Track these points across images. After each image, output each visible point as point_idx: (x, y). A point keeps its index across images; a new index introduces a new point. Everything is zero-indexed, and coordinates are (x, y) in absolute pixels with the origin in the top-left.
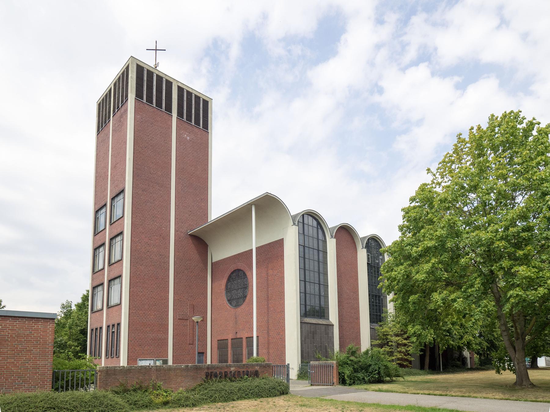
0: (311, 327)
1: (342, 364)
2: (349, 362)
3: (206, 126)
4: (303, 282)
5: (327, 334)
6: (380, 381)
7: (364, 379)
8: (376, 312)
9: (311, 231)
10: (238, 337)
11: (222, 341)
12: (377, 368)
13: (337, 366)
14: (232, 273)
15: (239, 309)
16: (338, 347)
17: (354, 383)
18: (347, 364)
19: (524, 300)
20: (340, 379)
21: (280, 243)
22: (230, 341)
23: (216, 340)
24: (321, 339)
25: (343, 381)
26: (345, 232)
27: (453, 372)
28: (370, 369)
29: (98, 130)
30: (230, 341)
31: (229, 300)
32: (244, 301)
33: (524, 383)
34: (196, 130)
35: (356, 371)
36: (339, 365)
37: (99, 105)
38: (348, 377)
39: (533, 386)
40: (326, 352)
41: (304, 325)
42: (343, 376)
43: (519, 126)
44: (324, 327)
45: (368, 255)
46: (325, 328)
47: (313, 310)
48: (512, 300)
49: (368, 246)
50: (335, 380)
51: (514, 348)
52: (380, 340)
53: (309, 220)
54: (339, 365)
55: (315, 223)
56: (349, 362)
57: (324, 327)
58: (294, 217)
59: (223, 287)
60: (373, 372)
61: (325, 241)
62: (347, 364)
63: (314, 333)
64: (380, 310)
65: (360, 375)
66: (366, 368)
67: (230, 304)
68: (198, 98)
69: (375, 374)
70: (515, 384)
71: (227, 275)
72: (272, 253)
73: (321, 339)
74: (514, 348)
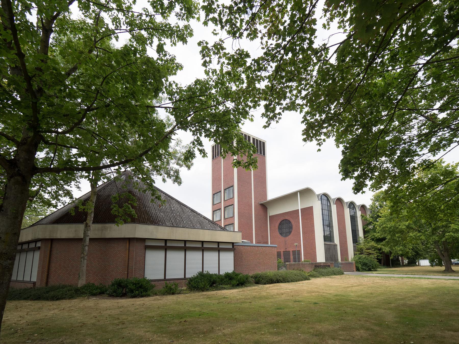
3: (264, 154)
5: (335, 249)
6: (370, 270)
9: (325, 202)
12: (371, 264)
15: (287, 238)
16: (16, 258)
19: (454, 237)
21: (311, 208)
22: (282, 253)
25: (358, 270)
27: (395, 267)
29: (213, 158)
30: (282, 253)
32: (290, 234)
33: (449, 270)
34: (260, 156)
37: (213, 147)
39: (453, 271)
43: (342, 12)
47: (328, 238)
48: (447, 237)
49: (349, 207)
51: (443, 256)
52: (358, 251)
53: (324, 197)
55: (326, 199)
57: (333, 246)
58: (318, 196)
59: (277, 227)
63: (329, 249)
68: (260, 142)
70: (445, 270)
71: (279, 222)
72: (308, 212)
74: (443, 256)
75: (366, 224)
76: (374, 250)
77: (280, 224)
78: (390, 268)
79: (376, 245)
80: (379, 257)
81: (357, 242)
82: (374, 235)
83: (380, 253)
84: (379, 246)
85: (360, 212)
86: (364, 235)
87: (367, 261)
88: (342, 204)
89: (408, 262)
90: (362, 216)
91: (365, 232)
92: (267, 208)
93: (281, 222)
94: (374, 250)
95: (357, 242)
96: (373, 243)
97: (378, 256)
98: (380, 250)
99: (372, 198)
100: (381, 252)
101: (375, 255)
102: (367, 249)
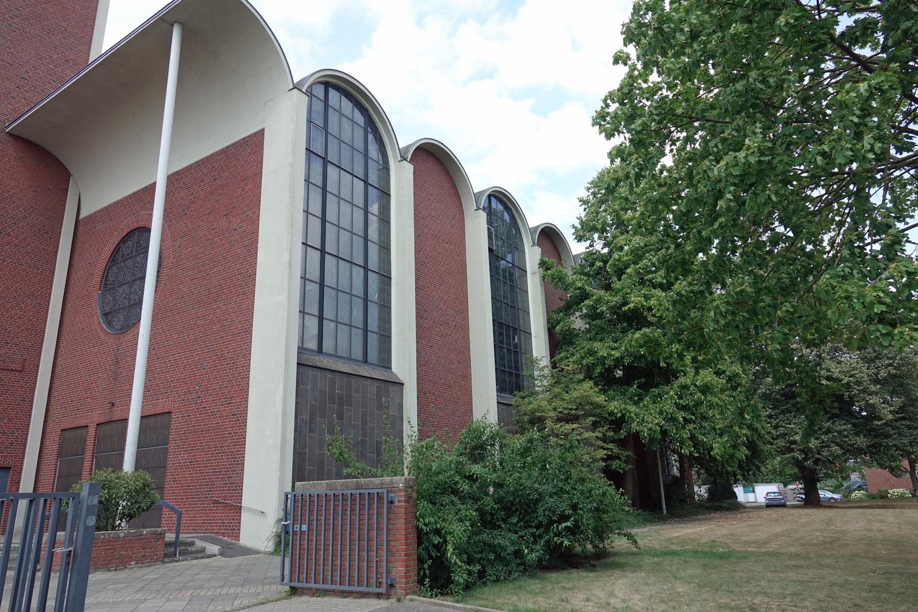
0: (332, 382)
1: (434, 491)
2: (465, 487)
4: (317, 254)
7: (518, 553)
8: (510, 367)
10: (115, 417)
11: (73, 433)
12: (564, 507)
13: (409, 499)
14: (124, 240)
17: (482, 574)
18: (455, 492)
20: (421, 561)
23: (58, 430)
24: (364, 421)
26: (434, 159)
28: (541, 515)
30: (92, 430)
31: (106, 315)
35: (487, 521)
36: (421, 496)
38: (460, 550)
40: (377, 452)
41: (311, 373)
42: (437, 547)
44: (373, 387)
45: (489, 229)
46: (379, 389)
50: (399, 570)
54: (421, 496)
56: (465, 487)
57: (373, 387)
60: (551, 523)
61: (386, 169)
62: (455, 492)
64: (516, 362)
65: (505, 539)
66: (517, 508)
67: (109, 324)
69: (558, 534)
73: (364, 421)
75: (560, 309)
76: (595, 425)
77: (113, 259)
78: (662, 519)
79: (600, 399)
80: (615, 464)
81: (519, 388)
82: (591, 353)
83: (621, 443)
84: (615, 406)
85: (538, 250)
86: (552, 355)
87: (531, 481)
88: (457, 196)
89: (709, 491)
90: (543, 264)
91: (559, 341)
92: (68, 175)
93: (117, 249)
94: (595, 425)
95: (519, 388)
96: (587, 389)
97: (609, 458)
98: (618, 422)
99: (585, 194)
100: (623, 433)
101: (591, 449)
102: (559, 420)
